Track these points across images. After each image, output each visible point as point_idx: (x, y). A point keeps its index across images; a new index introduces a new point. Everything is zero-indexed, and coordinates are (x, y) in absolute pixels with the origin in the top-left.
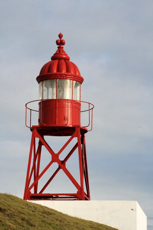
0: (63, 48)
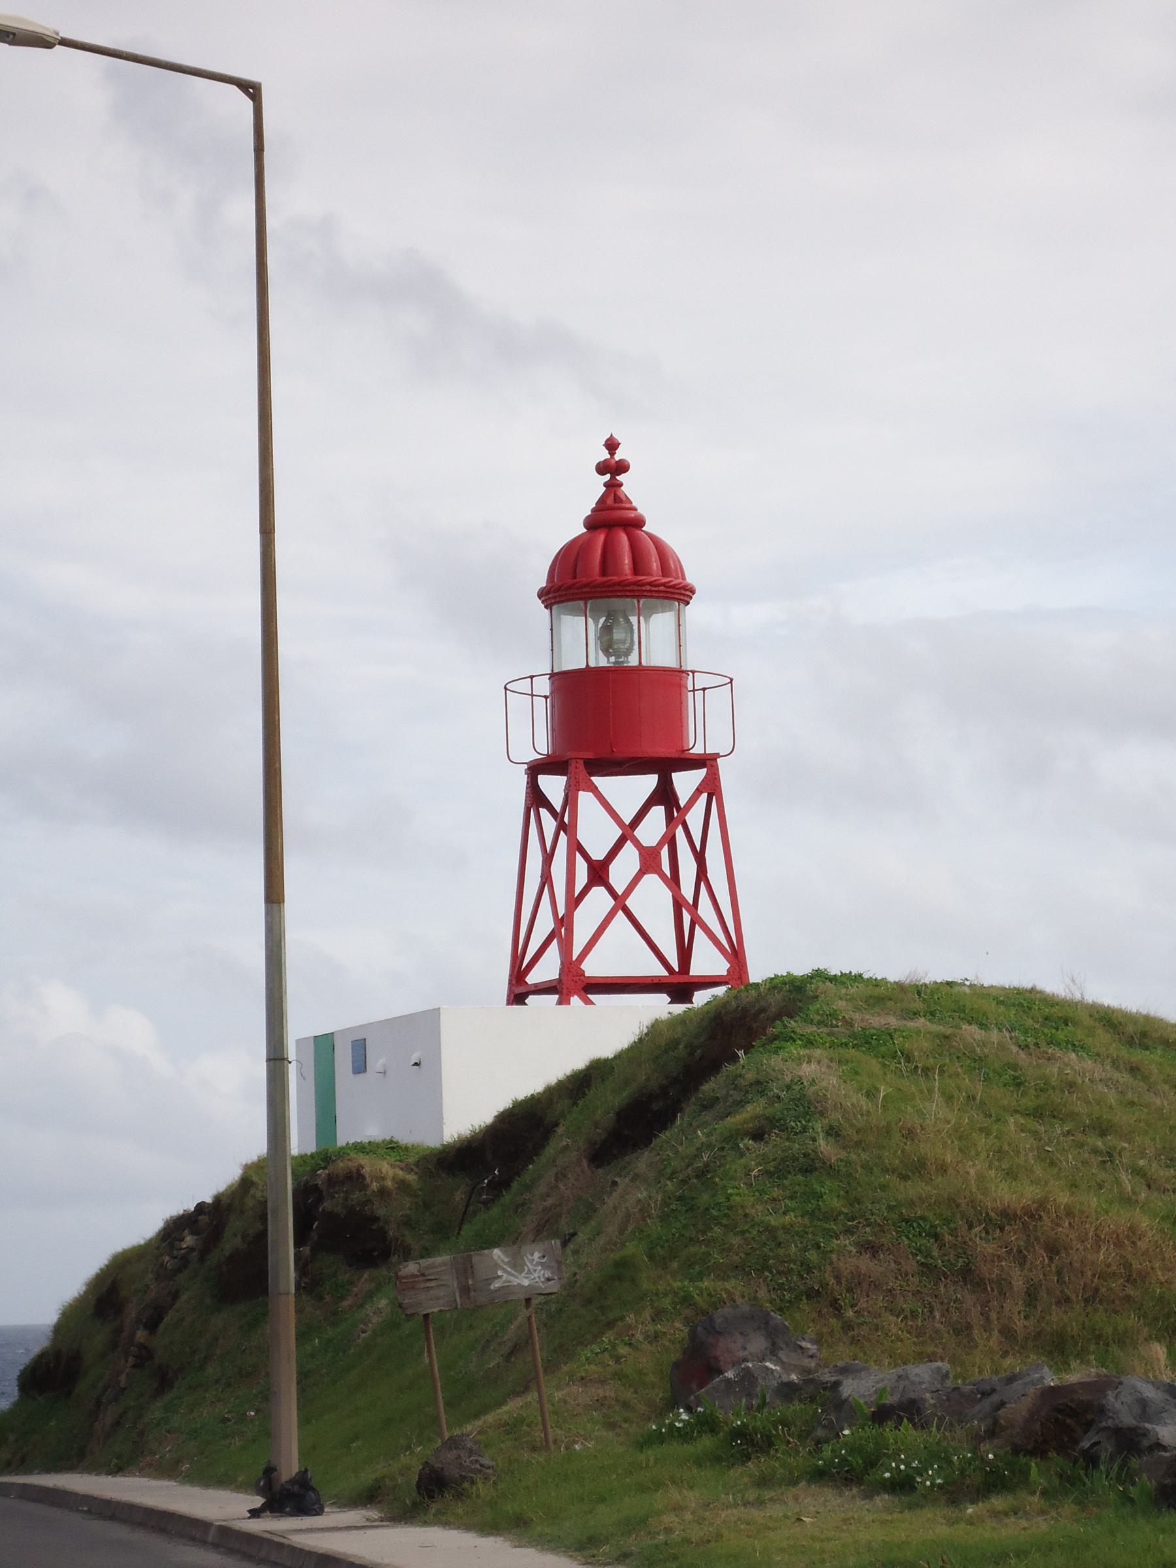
0: (621, 485)
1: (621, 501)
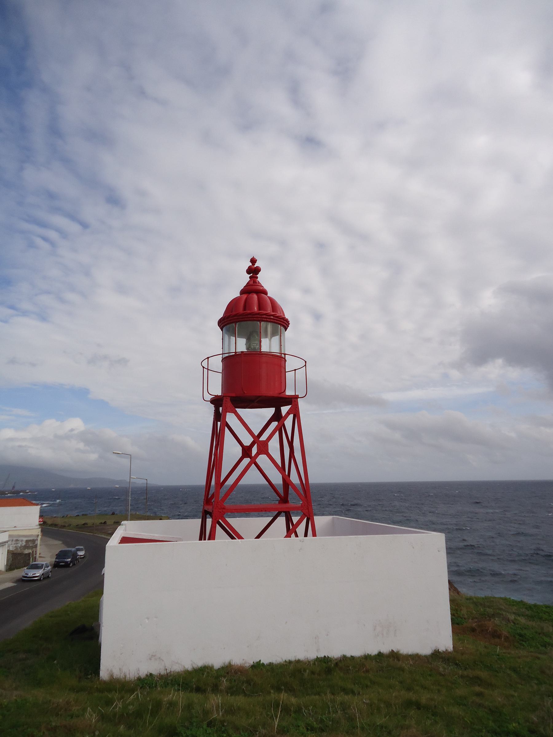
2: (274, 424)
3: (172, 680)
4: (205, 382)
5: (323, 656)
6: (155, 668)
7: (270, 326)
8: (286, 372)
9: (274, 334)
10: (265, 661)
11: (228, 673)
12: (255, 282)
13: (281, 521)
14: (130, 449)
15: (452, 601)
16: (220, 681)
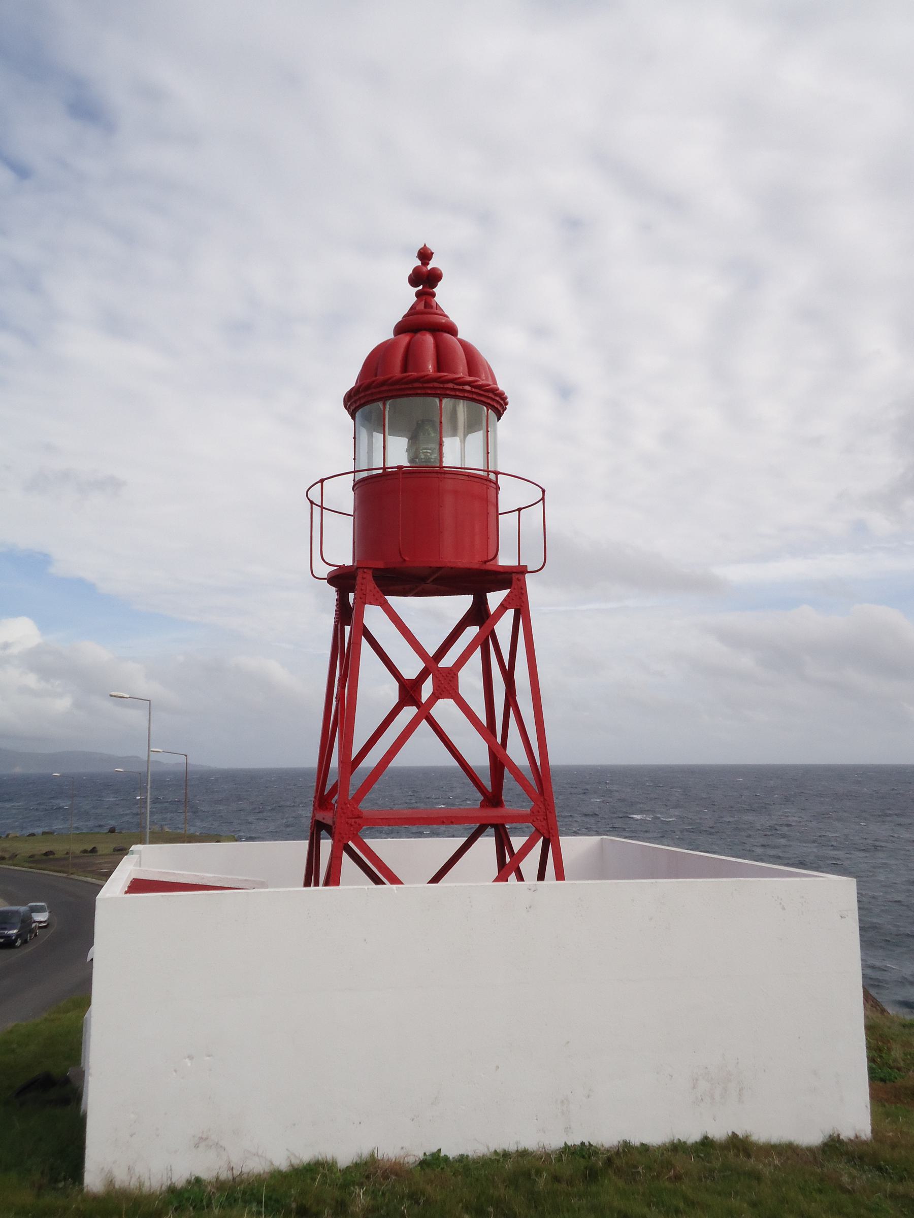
1: (431, 307)
2: (472, 632)
3: (244, 1193)
4: (316, 540)
5: (578, 1143)
6: (207, 1166)
7: (462, 408)
8: (498, 514)
9: (472, 426)
10: (451, 1151)
11: (368, 1177)
12: (428, 305)
13: (487, 845)
14: (144, 687)
15: (870, 1029)
16: (350, 1194)
